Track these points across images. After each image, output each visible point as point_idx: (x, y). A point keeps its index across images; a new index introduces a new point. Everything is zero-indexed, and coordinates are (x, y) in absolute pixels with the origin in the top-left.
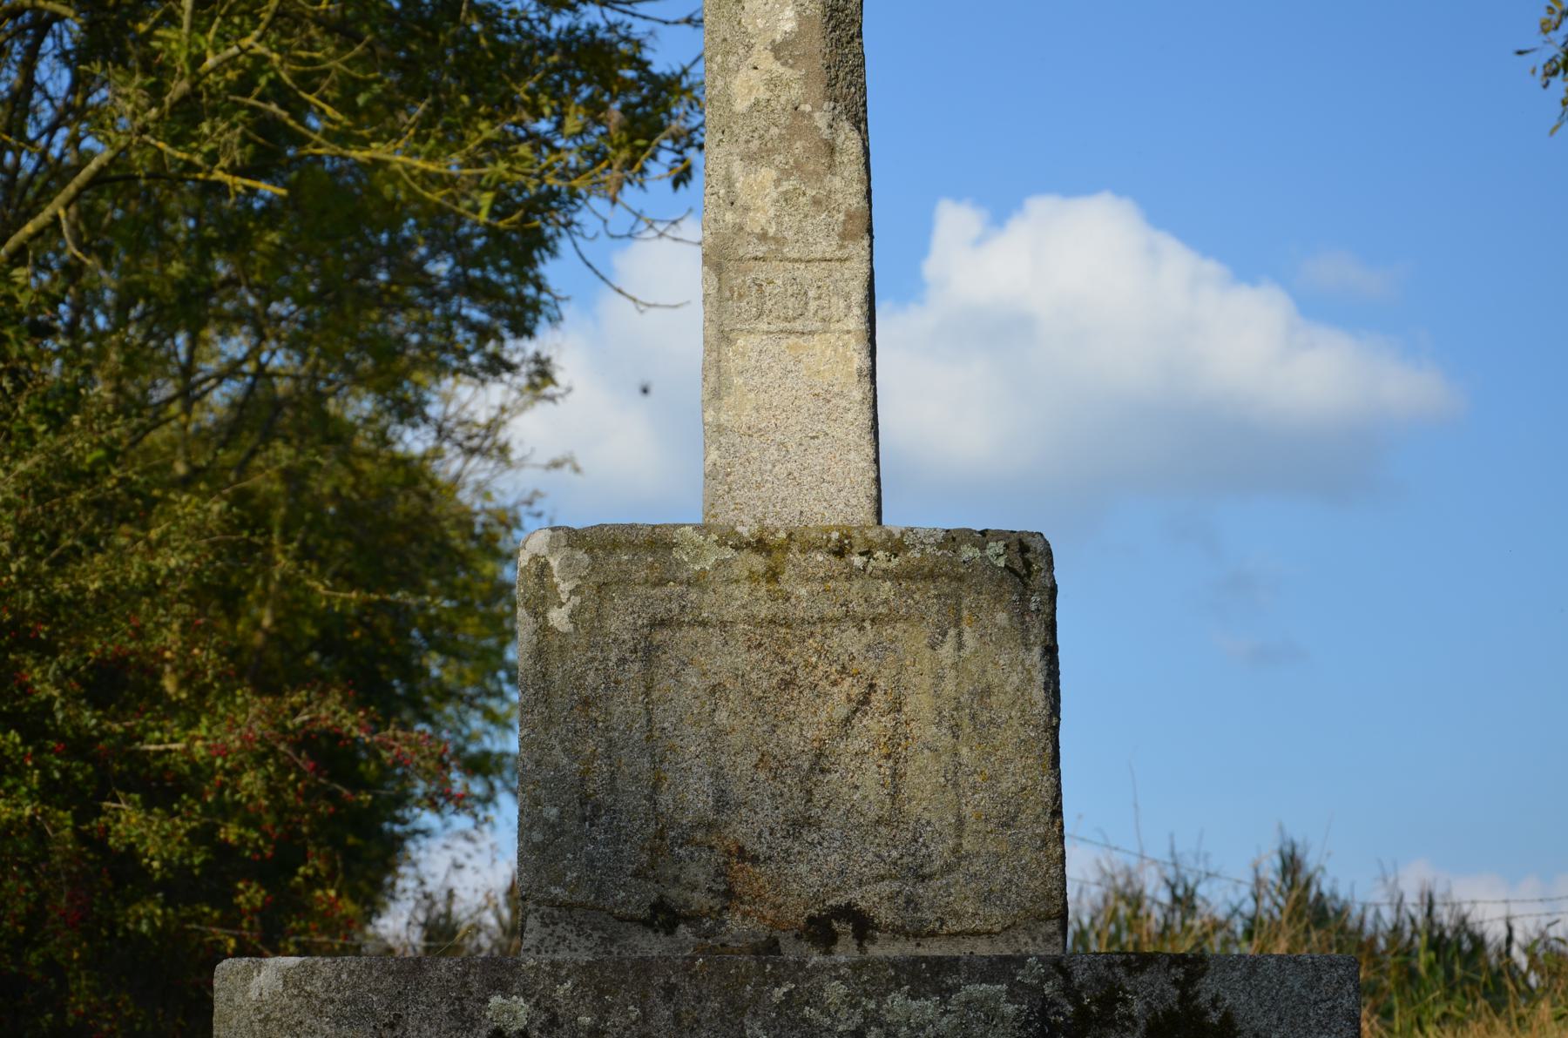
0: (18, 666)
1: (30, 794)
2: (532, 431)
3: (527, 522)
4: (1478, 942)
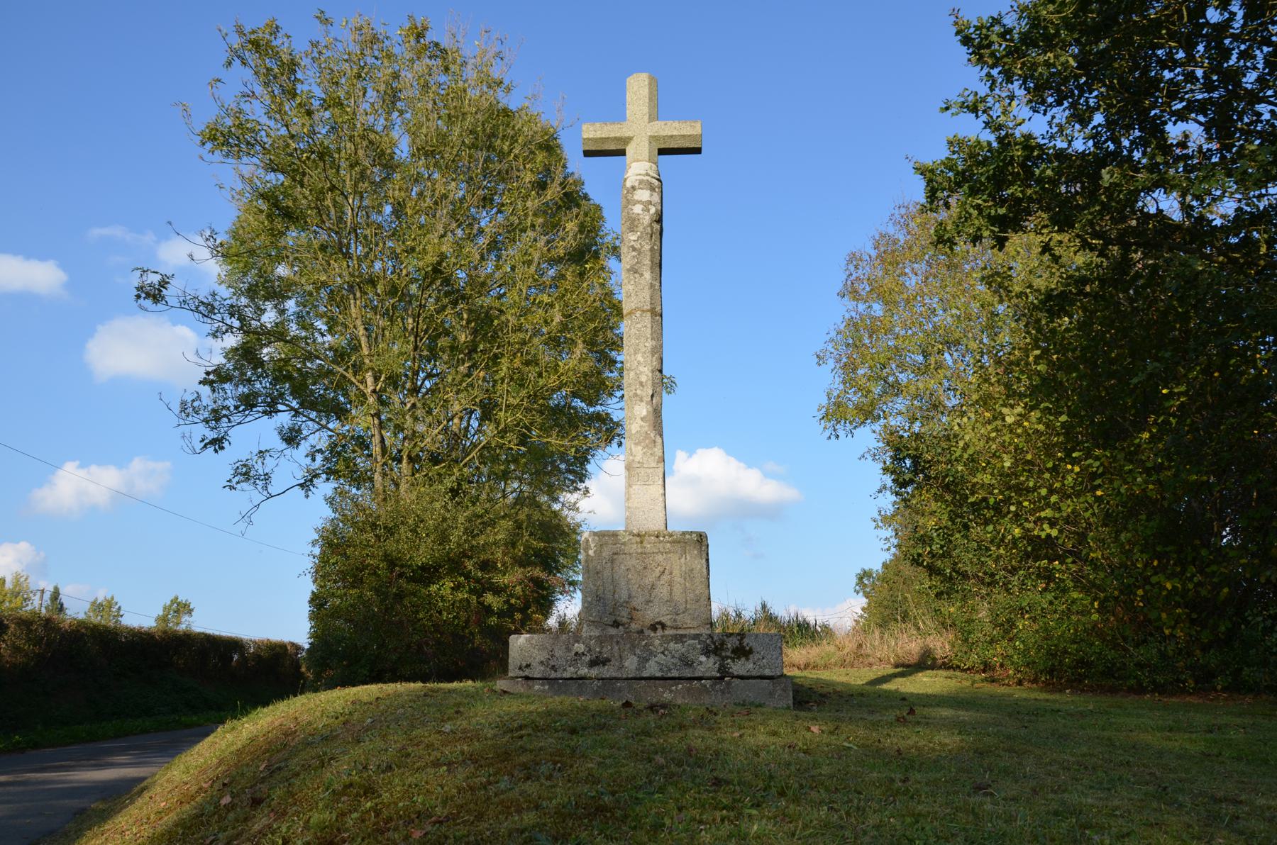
2: (584, 504)
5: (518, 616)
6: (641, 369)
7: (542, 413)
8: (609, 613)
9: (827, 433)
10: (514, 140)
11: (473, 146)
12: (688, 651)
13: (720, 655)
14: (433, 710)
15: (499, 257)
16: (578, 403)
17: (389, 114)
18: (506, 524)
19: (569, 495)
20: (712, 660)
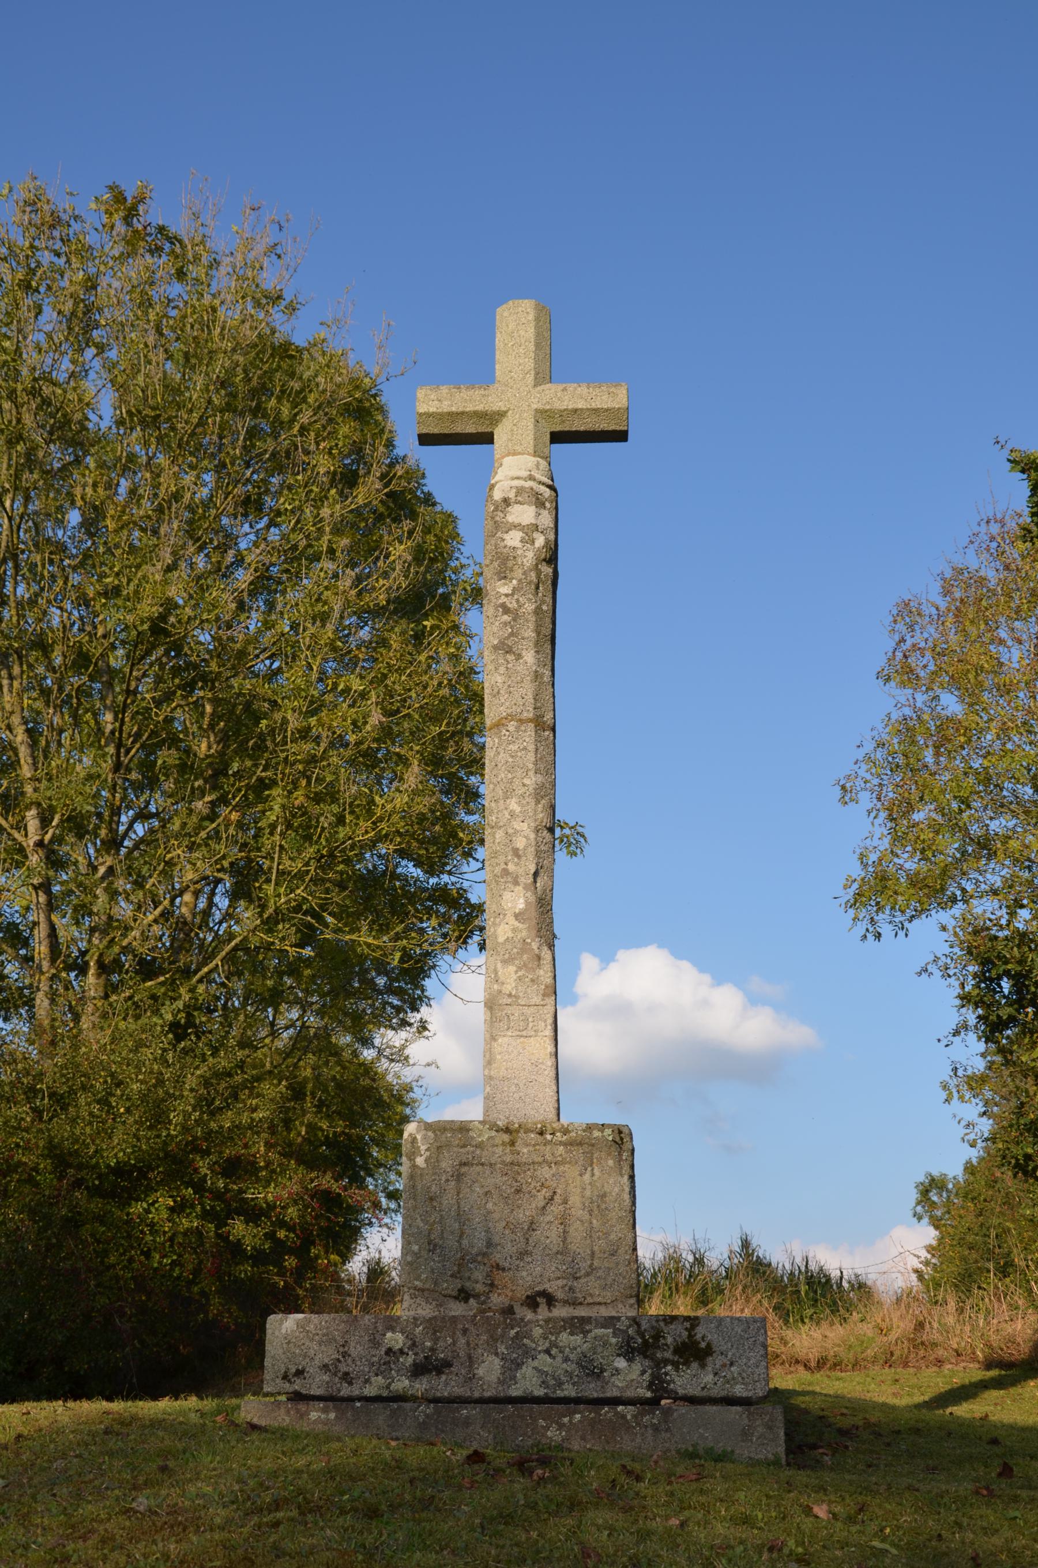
0: (193, 1160)
1: (196, 1217)
2: (418, 1050)
3: (416, 1089)
4: (828, 1279)
5: (290, 1262)
6: (517, 825)
7: (342, 886)
8: (456, 1265)
9: (861, 928)
10: (298, 399)
11: (229, 408)
12: (594, 1349)
13: (652, 1358)
14: (118, 1464)
15: (271, 606)
16: (410, 870)
17: (81, 351)
18: (272, 1090)
19: (390, 1033)
20: (637, 1367)
